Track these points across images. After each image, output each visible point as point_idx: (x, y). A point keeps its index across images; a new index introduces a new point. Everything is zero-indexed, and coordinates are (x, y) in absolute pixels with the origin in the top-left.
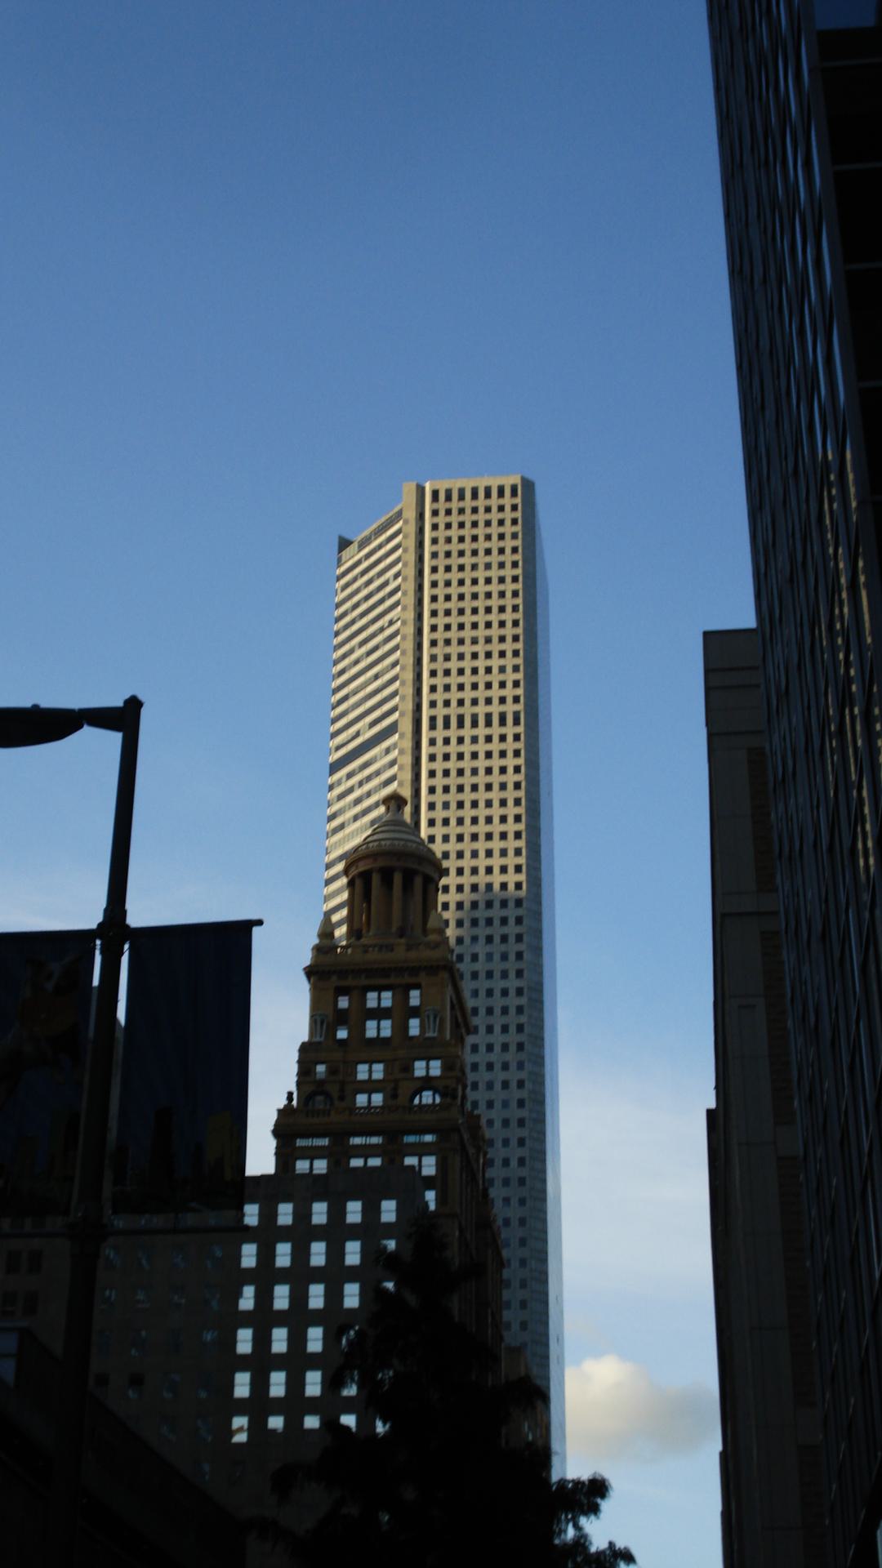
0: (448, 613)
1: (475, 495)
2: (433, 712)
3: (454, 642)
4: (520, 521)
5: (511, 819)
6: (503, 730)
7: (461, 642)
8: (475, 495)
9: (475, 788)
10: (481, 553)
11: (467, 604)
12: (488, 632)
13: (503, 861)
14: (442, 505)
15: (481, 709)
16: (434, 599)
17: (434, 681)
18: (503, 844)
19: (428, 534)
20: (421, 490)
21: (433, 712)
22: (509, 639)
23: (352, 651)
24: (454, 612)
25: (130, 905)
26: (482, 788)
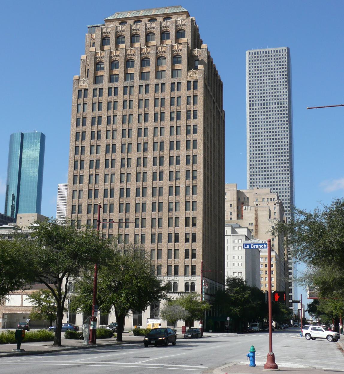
14: (251, 56)
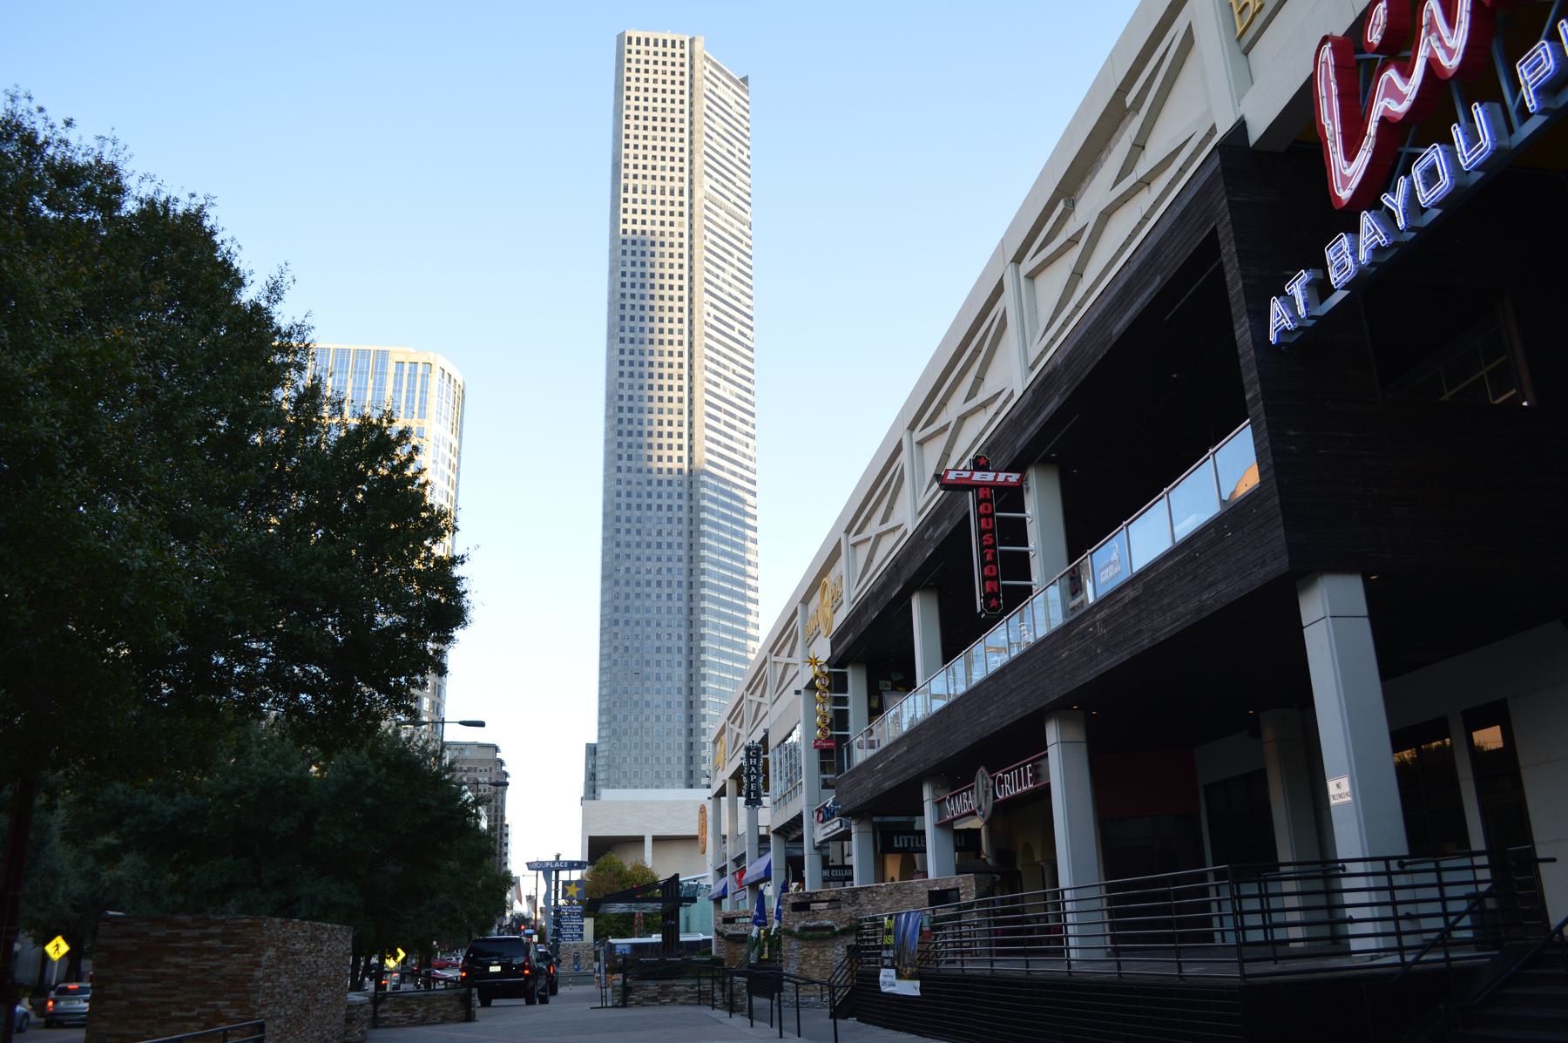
2: (682, 51)
5: (631, 156)
23: (726, 424)
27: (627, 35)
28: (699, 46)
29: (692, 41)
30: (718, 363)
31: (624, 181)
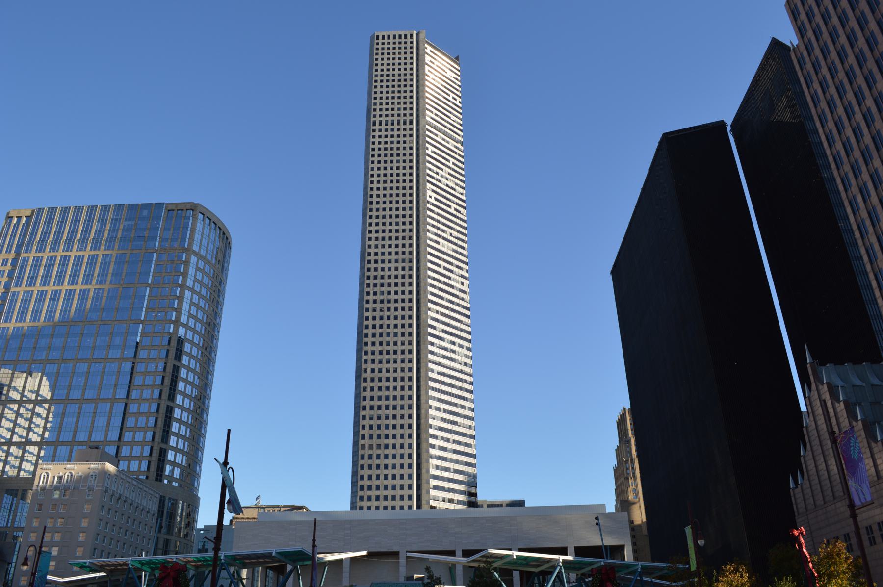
0: (404, 174)
1: (394, 37)
3: (400, 231)
4: (373, 87)
6: (380, 127)
7: (398, 195)
8: (394, 37)
9: (390, 238)
10: (389, 162)
11: (395, 199)
12: (383, 235)
13: (376, 250)
15: (390, 119)
16: (411, 168)
17: (410, 356)
18: (373, 340)
19: (414, 50)
20: (419, 506)
21: (411, 126)
22: (375, 189)
24: (401, 216)
25: (627, 515)
26: (387, 238)
27: (376, 34)
28: (422, 36)
29: (417, 35)
30: (438, 228)
31: (373, 119)
